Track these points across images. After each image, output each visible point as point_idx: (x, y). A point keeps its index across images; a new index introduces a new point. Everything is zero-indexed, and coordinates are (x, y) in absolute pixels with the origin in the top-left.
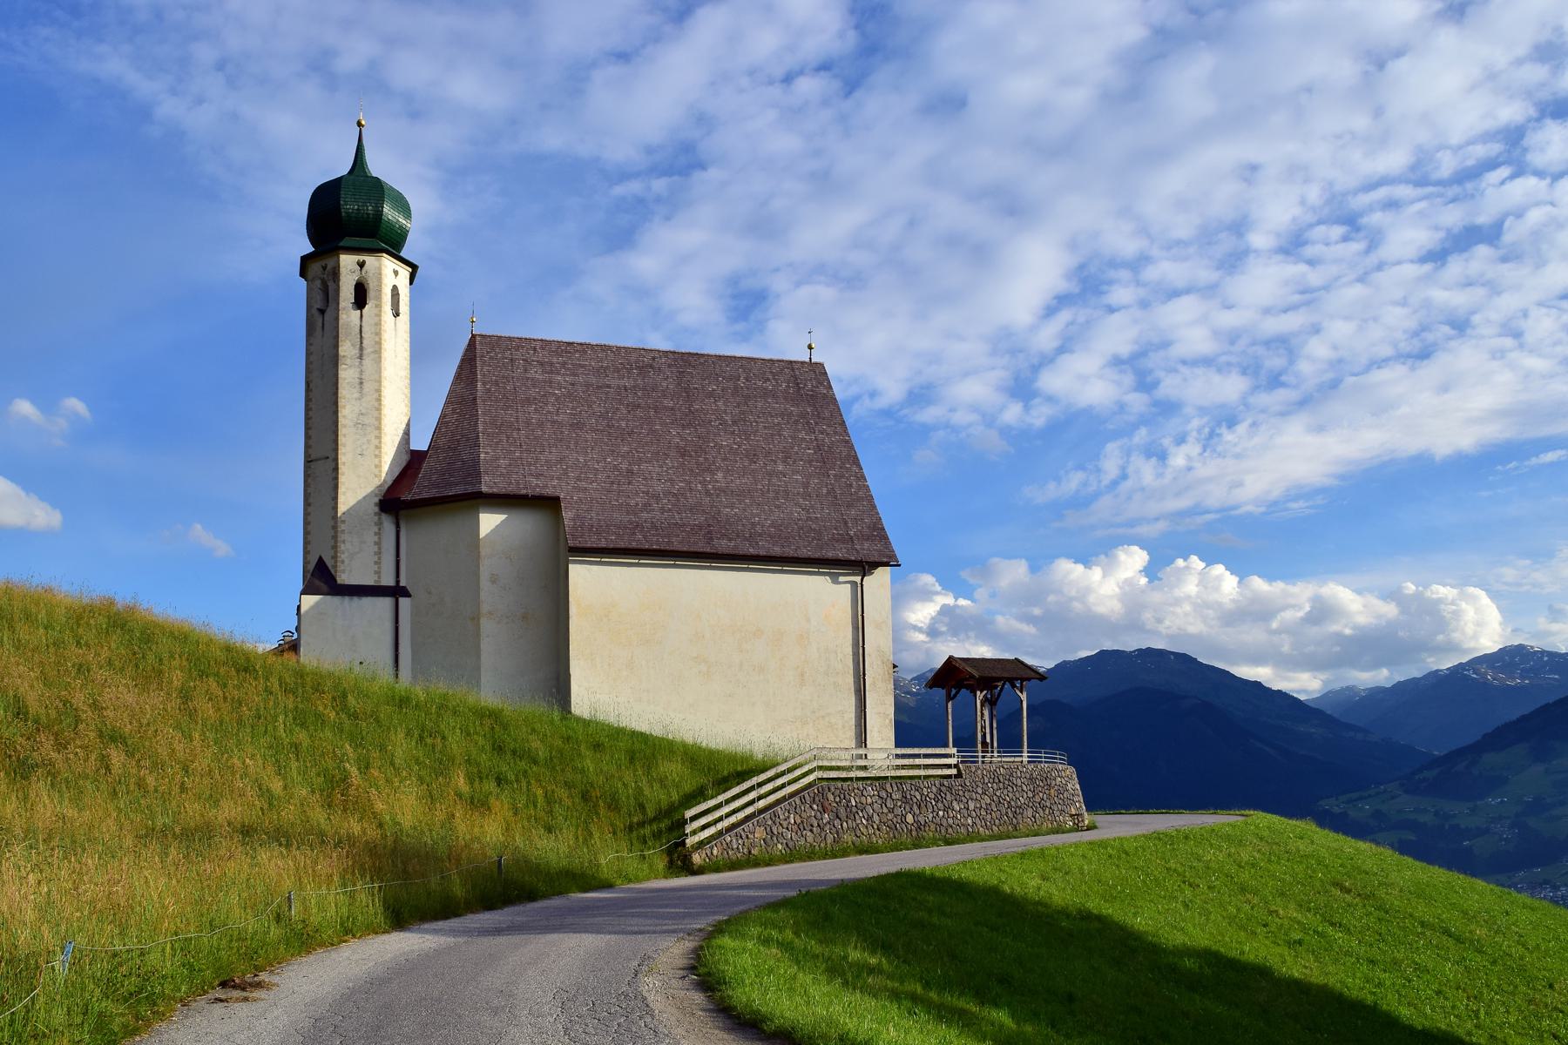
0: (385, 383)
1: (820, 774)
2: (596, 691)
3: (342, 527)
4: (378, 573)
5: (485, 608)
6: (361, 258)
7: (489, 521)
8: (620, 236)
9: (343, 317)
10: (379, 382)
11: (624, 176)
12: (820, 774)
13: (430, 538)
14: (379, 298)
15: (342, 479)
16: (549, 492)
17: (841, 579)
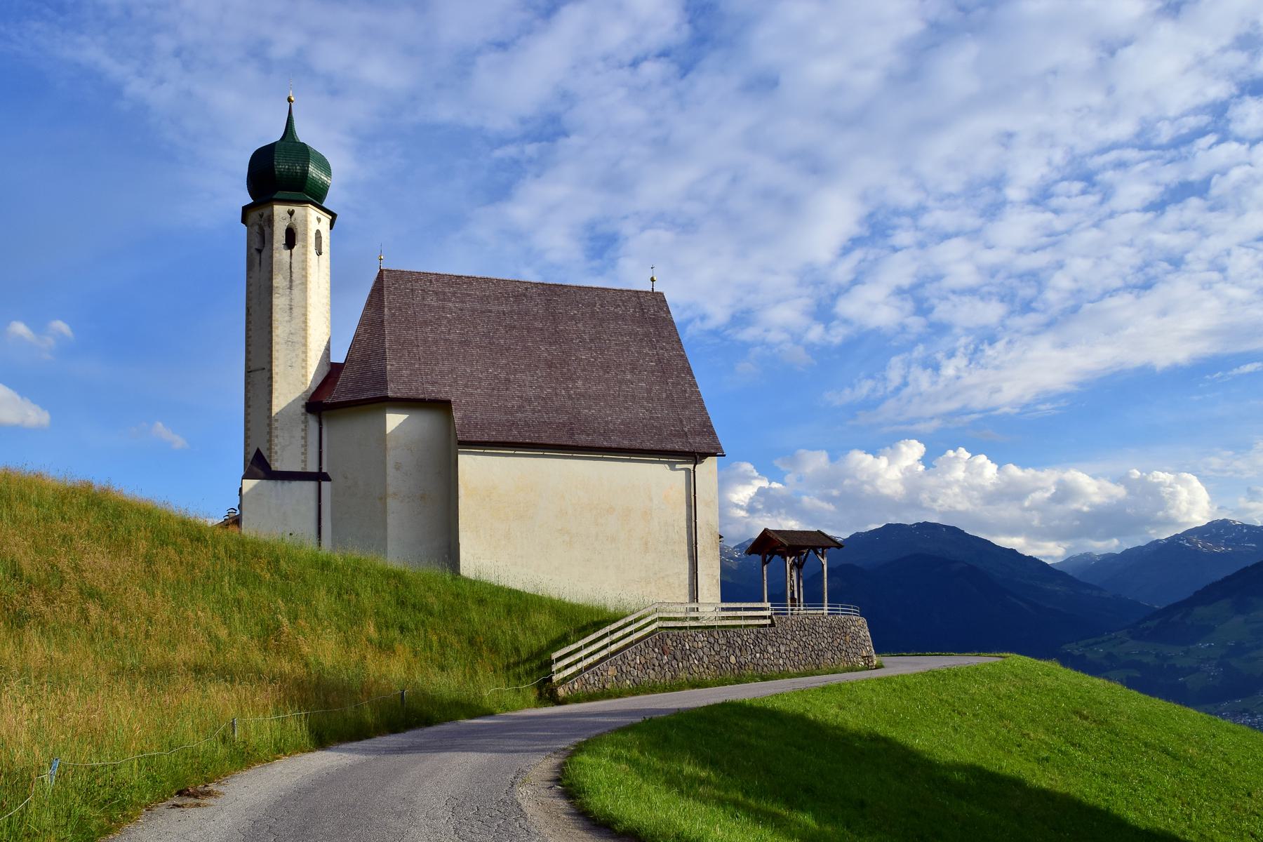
0: (310, 309)
1: (660, 624)
2: (480, 557)
3: (276, 425)
4: (304, 461)
5: (390, 490)
6: (291, 208)
7: (394, 420)
8: (500, 190)
9: (276, 255)
10: (306, 308)
11: (503, 141)
12: (660, 624)
13: (346, 434)
14: (305, 240)
15: (275, 386)
16: (442, 396)
17: (678, 466)
